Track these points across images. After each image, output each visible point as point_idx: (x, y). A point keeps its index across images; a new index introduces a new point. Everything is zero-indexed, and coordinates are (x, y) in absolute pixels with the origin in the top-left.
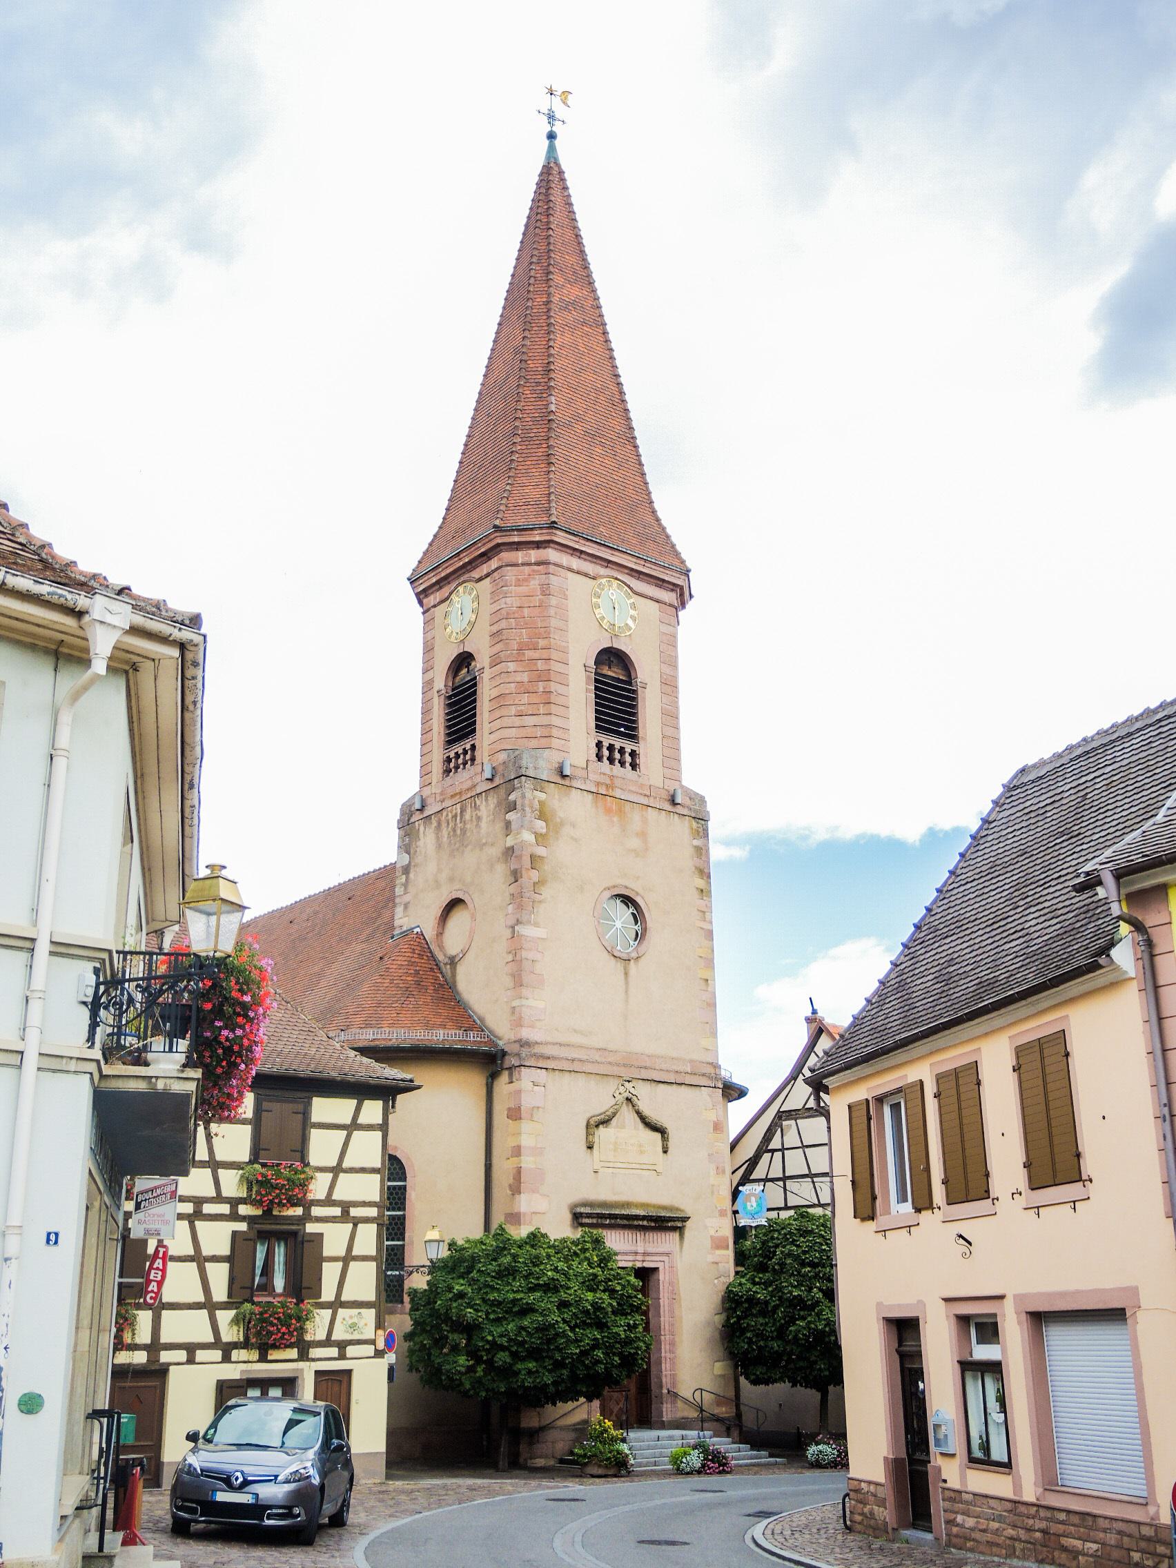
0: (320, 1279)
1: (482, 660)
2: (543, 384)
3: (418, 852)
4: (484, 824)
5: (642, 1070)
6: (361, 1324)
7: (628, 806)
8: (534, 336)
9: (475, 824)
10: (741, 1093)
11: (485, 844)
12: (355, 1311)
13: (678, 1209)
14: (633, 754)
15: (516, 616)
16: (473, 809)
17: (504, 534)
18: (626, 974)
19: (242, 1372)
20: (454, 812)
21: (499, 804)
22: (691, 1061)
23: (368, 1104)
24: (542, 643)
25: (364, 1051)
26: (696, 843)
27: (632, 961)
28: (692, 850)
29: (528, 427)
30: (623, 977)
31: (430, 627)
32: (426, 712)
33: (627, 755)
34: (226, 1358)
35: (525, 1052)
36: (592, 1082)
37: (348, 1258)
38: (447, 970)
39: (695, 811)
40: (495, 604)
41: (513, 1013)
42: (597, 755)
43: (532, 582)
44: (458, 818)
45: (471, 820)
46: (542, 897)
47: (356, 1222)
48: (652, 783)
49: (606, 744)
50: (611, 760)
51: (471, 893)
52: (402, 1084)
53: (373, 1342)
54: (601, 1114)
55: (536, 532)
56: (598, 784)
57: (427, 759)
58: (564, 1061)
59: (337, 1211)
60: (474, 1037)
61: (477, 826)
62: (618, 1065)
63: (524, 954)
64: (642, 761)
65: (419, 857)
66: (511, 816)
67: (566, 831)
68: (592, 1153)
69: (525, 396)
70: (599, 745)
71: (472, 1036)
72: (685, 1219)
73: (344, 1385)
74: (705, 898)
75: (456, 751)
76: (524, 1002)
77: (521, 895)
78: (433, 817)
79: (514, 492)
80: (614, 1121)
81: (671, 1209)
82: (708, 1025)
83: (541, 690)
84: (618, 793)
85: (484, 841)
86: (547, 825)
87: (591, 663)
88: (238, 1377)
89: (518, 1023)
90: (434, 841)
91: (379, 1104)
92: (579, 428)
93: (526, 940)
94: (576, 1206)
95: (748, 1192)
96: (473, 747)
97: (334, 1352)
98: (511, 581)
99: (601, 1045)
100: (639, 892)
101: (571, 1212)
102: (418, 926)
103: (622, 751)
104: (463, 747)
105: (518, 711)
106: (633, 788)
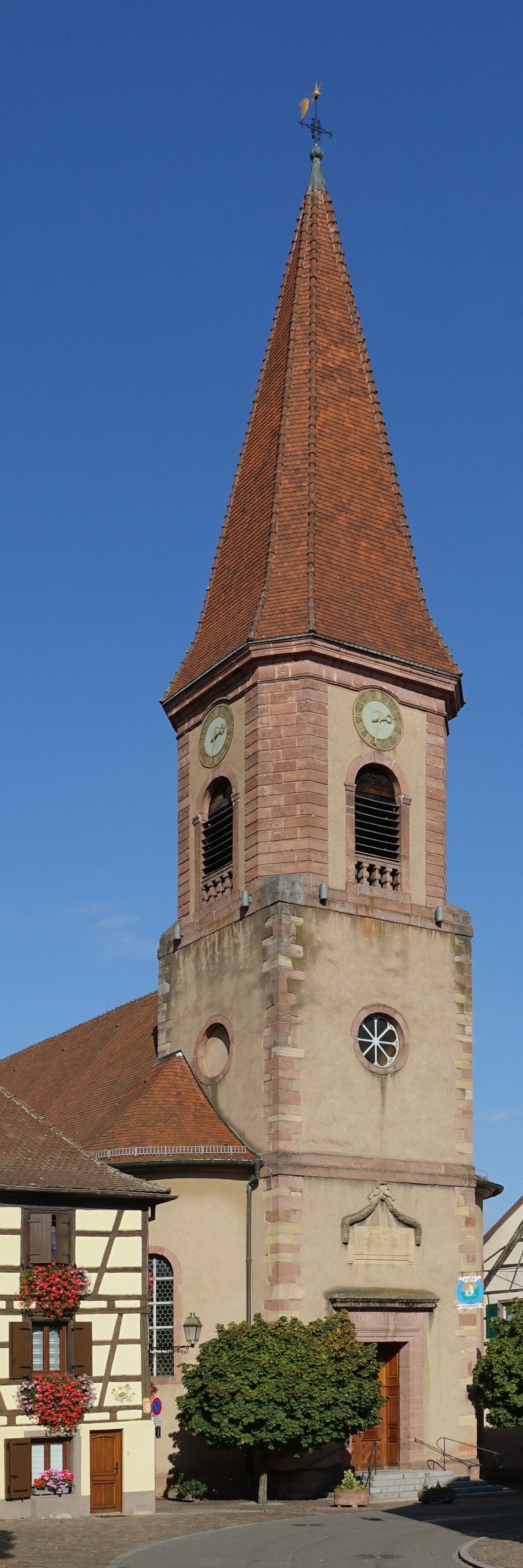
0: (91, 1359)
1: (239, 787)
2: (302, 471)
3: (178, 981)
4: (241, 952)
5: (397, 1174)
6: (130, 1393)
7: (388, 926)
8: (293, 413)
9: (232, 951)
10: (497, 1190)
11: (242, 971)
12: (124, 1384)
13: (428, 1293)
14: (394, 873)
15: (273, 736)
16: (231, 937)
17: (259, 647)
18: (383, 1088)
19: (26, 1432)
20: (212, 940)
21: (256, 930)
22: (446, 1165)
23: (127, 1213)
24: (299, 763)
25: (124, 1168)
26: (457, 959)
27: (389, 1075)
28: (452, 967)
29: (286, 523)
30: (379, 1091)
31: (185, 752)
32: (183, 841)
33: (388, 874)
34: (11, 1423)
35: (281, 1162)
36: (348, 1187)
37: (115, 1342)
38: (208, 1090)
39: (460, 927)
40: (249, 725)
41: (270, 1128)
42: (357, 877)
43: (289, 699)
44: (216, 947)
45: (229, 947)
46: (299, 1019)
47: (121, 1312)
48: (414, 902)
49: (366, 865)
50: (371, 881)
51: (229, 1018)
52: (159, 1196)
53: (140, 1407)
54: (356, 1214)
55: (293, 643)
56: (357, 906)
57: (183, 889)
58: (321, 1169)
59: (103, 1304)
60: (233, 1151)
61: (236, 953)
62: (372, 1170)
63: (281, 1073)
64: (402, 879)
65: (179, 986)
66: (268, 942)
67: (325, 954)
68: (346, 1248)
69: (282, 487)
70: (359, 866)
71: (231, 1150)
72: (435, 1301)
73: (117, 1440)
74: (465, 1012)
75: (213, 879)
76: (281, 1117)
77: (277, 1018)
78: (192, 946)
79: (270, 599)
80: (369, 1220)
81: (422, 1292)
82: (463, 1131)
83: (298, 812)
84: (378, 914)
85: (242, 968)
86: (304, 949)
87: (352, 780)
88: (22, 1436)
89: (276, 1136)
90: (193, 969)
91: (138, 1214)
92: (342, 520)
93: (282, 1060)
94: (332, 1293)
95: (467, 1281)
96: (230, 875)
97: (106, 1416)
98: (267, 699)
99: (358, 1153)
100: (398, 1010)
101: (326, 1298)
102: (180, 1051)
103: (382, 871)
104: (220, 875)
105: (275, 836)
106: (394, 909)
